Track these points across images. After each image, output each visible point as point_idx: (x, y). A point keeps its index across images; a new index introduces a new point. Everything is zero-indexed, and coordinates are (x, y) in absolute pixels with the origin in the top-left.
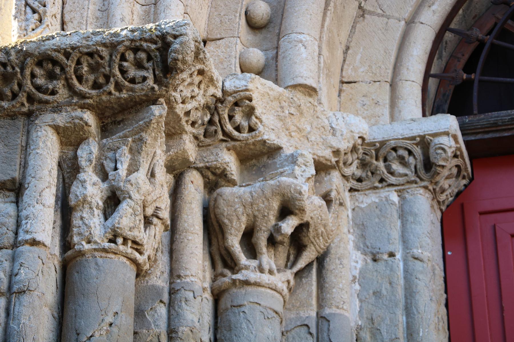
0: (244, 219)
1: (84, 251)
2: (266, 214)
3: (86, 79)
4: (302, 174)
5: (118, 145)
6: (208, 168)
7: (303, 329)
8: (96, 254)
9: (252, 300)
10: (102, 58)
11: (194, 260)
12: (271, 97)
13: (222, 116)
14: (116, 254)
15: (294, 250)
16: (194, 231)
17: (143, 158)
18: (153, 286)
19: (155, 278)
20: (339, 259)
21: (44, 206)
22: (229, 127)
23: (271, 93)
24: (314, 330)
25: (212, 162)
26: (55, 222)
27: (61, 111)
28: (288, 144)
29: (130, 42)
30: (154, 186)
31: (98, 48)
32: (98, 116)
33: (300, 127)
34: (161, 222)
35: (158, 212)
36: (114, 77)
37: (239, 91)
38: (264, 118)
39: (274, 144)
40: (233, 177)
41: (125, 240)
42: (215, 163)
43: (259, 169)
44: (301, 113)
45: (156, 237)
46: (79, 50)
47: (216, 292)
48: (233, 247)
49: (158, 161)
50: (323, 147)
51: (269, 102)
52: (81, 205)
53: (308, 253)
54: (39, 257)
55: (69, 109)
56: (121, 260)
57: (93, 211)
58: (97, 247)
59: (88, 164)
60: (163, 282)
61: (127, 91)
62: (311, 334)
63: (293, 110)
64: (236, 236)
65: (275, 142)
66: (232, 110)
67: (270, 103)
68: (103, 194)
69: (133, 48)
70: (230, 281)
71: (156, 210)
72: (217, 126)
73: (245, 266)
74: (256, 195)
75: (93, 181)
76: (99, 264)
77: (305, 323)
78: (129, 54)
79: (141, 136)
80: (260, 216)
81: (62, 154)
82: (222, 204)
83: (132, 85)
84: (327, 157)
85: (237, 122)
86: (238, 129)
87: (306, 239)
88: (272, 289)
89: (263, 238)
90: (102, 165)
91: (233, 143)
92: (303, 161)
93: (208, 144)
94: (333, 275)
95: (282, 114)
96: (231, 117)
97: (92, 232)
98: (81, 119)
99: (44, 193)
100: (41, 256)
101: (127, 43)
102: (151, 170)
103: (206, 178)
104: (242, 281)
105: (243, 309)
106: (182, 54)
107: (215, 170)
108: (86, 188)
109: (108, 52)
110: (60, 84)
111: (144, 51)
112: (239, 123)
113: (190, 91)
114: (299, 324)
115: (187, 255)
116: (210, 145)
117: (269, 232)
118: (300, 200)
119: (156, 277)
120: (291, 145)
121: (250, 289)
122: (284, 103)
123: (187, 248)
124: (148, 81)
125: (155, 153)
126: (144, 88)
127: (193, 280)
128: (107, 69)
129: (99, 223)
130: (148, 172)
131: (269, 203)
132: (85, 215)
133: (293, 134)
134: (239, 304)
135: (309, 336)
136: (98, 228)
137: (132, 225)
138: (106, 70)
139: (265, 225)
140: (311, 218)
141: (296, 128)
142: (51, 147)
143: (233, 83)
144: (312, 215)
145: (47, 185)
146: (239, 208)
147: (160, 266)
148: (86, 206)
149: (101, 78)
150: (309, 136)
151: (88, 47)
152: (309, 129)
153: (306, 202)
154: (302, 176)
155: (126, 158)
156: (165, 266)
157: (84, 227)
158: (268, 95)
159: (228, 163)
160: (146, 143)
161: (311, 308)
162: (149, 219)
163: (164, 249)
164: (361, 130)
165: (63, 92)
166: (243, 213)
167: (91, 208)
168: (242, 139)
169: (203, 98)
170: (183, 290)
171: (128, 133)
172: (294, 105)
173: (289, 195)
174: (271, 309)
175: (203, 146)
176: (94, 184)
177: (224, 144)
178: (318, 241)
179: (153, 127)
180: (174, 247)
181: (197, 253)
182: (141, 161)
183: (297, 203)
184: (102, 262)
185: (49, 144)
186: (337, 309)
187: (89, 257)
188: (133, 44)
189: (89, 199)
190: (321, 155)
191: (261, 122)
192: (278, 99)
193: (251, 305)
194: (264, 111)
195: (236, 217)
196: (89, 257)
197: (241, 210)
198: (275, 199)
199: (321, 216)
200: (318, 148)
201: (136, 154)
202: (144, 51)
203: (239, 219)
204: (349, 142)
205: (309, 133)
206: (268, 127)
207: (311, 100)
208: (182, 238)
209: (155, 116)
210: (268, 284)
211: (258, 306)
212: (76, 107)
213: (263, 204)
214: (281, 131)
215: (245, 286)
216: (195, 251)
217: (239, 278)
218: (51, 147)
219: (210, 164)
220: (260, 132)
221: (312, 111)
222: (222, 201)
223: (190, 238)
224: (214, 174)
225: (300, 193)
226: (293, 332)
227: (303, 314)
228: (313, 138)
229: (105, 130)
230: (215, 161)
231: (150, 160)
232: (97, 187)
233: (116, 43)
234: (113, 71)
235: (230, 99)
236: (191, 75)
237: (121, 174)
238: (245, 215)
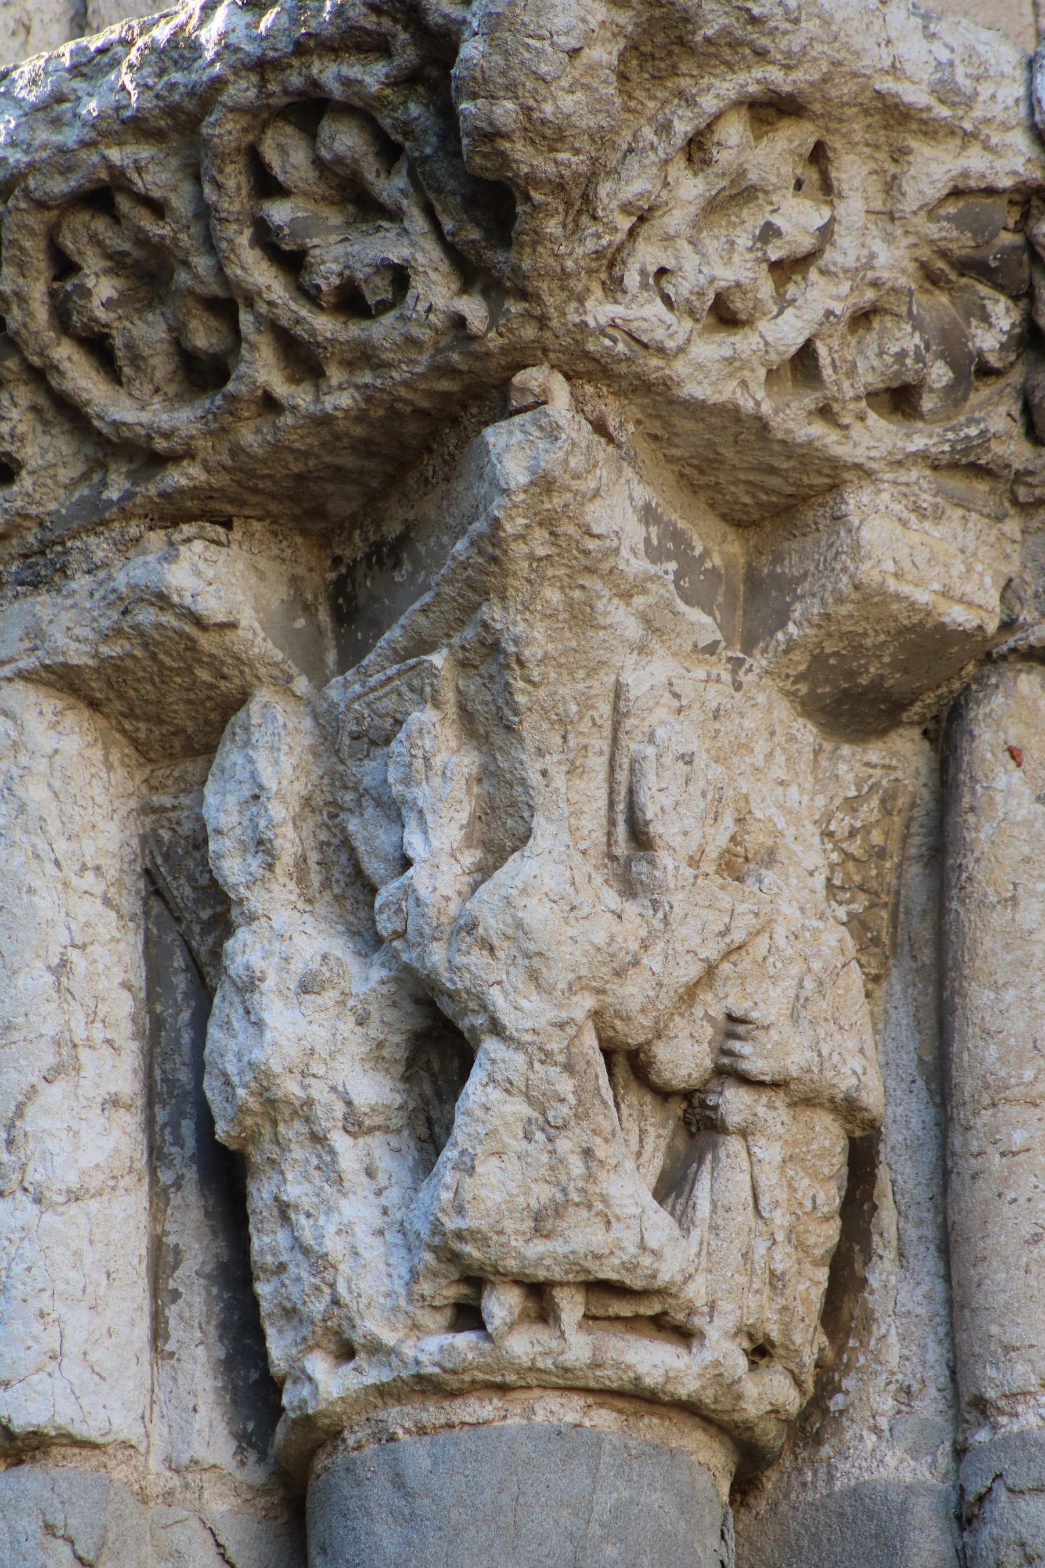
1: (324, 1414)
3: (127, 346)
5: (389, 704)
8: (397, 1417)
10: (158, 208)
14: (503, 1389)
17: (540, 753)
18: (856, 1493)
19: (870, 1440)
21: (38, 1201)
26: (161, 1261)
27: (63, 570)
29: (254, 78)
30: (655, 904)
31: (115, 155)
32: (305, 533)
34: (780, 1100)
35: (737, 1046)
36: (250, 304)
41: (539, 1297)
45: (764, 1201)
46: (26, 191)
49: (651, 739)
52: (267, 1131)
54: (49, 1529)
55: (100, 548)
56: (539, 1418)
57: (332, 1152)
58: (385, 1376)
59: (255, 863)
60: (914, 1452)
61: (350, 365)
68: (374, 1030)
69: (288, 106)
71: (732, 1035)
75: (297, 967)
76: (412, 1483)
78: (282, 149)
79: (485, 626)
81: (148, 820)
83: (355, 330)
90: (346, 844)
97: (342, 1289)
98: (162, 600)
99: (32, 1122)
100: (58, 1520)
101: (242, 90)
102: (621, 807)
106: (512, 89)
108: (259, 1025)
109: (174, 162)
110: (15, 414)
111: (347, 110)
113: (744, 241)
115: (1005, 1261)
119: (876, 1430)
123: (1008, 1211)
124: (418, 285)
125: (619, 691)
126: (416, 331)
128: (202, 263)
129: (379, 1222)
130: (612, 822)
132: (294, 1191)
136: (373, 1251)
137: (543, 1193)
138: (196, 277)
142: (51, 811)
145: (49, 1059)
147: (893, 1356)
148: (292, 1131)
149: (193, 324)
151: (63, 160)
155: (437, 781)
156: (923, 1347)
157: (300, 1269)
160: (521, 664)
162: (703, 1104)
163: (912, 1233)
165: (44, 452)
167: (318, 1139)
169: (889, 239)
170: (1003, 1496)
171: (421, 620)
176: (307, 986)
179: (531, 557)
180: (953, 1216)
182: (535, 778)
184: (427, 1463)
185: (36, 793)
187: (359, 1447)
188: (273, 87)
189: (291, 1087)
196: (359, 1447)
201: (499, 737)
202: (347, 110)
208: (974, 1147)
209: (506, 492)
212: (133, 530)
218: (51, 811)
223: (1019, 1138)
229: (347, 610)
231: (600, 743)
232: (330, 997)
233: (190, 105)
234: (233, 271)
236: (697, 149)
237: (423, 892)
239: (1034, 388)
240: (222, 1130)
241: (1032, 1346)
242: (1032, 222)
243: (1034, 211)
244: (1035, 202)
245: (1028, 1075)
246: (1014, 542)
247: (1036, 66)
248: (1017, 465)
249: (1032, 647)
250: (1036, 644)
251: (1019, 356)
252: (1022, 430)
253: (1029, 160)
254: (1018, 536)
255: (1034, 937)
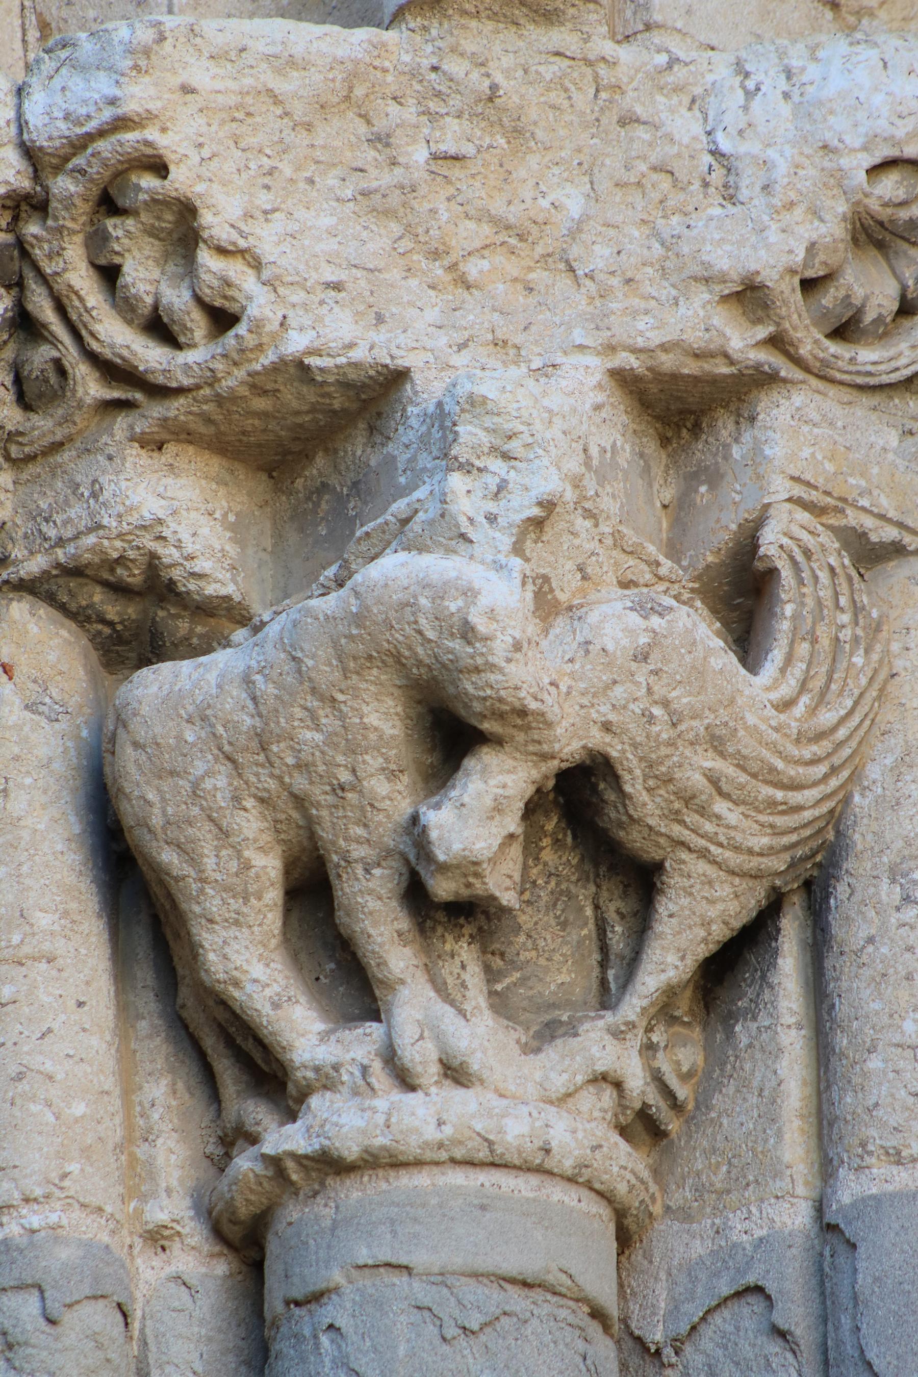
0: (250, 824)
2: (345, 776)
4: (491, 506)
6: (75, 571)
7: (746, 1310)
9: (364, 1255)
11: (34, 1108)
12: (299, 110)
13: (59, 286)
15: (625, 895)
16: (26, 949)
20: (894, 874)
22: (116, 335)
23: (281, 86)
24: (796, 1313)
25: (76, 537)
28: (442, 340)
33: (513, 214)
37: (90, 138)
38: (266, 239)
39: (355, 365)
40: (211, 589)
42: (91, 540)
43: (342, 501)
44: (517, 133)
47: (234, 1233)
48: (237, 984)
50: (667, 292)
51: (289, 137)
53: (685, 901)
62: (781, 1334)
63: (452, 135)
64: (237, 923)
65: (359, 354)
66: (97, 240)
67: (301, 139)
70: (259, 1168)
72: (53, 341)
73: (317, 1069)
74: (271, 690)
77: (751, 1279)
80: (319, 793)
82: (132, 769)
84: (696, 338)
85: (138, 299)
86: (160, 328)
87: (635, 835)
88: (470, 1163)
89: (372, 904)
91: (157, 410)
92: (485, 439)
93: (45, 442)
94: (866, 972)
95: (384, 179)
96: (109, 275)
103: (88, 619)
104: (306, 1157)
105: (328, 1313)
107: (112, 570)
112: (149, 300)
114: (726, 1291)
116: (57, 447)
117: (396, 863)
118: (477, 670)
120: (459, 337)
121: (352, 1193)
122: (393, 108)
127: (35, 1221)
131: (342, 717)
133: (474, 268)
134: (311, 1288)
135: (774, 1347)
139: (360, 831)
140: (607, 727)
141: (486, 229)
143: (59, 99)
144: (604, 711)
146: (208, 774)
150: (575, 251)
152: (574, 203)
153: (511, 668)
154: (492, 519)
158: (276, 100)
159: (160, 521)
161: (782, 1185)
164: (882, 125)
166: (236, 799)
168: (186, 382)
172: (456, 102)
173: (420, 650)
174: (476, 1275)
175: (31, 458)
177: (121, 423)
178: (709, 827)
181: (49, 1067)
183: (470, 689)
186: (895, 1169)
190: (656, 338)
191: (257, 265)
192: (349, 95)
193: (365, 1281)
194: (264, 200)
195: (208, 826)
197: (221, 781)
198: (368, 688)
199: (665, 704)
200: (636, 302)
203: (224, 833)
204: (815, 213)
205: (576, 231)
206: (301, 284)
207: (560, 37)
210: (441, 1145)
211: (400, 1280)
213: (318, 728)
214: (395, 274)
215: (329, 1181)
216: (36, 1061)
217: (287, 1147)
219: (71, 549)
220: (257, 327)
221: (583, 99)
222: (129, 750)
224: (119, 589)
225: (467, 633)
226: (708, 1338)
227: (743, 1229)
228: (599, 257)
230: (90, 530)
235: (63, 185)
238: (249, 803)
239: (23, 363)
240: (857, 1287)
241: (15, 1167)
242: (21, 224)
243: (23, 215)
244: (24, 207)
245: (16, 939)
246: (7, 491)
247: (24, 94)
248: (10, 427)
249: (21, 580)
250: (26, 577)
251: (11, 336)
252: (14, 398)
253: (18, 172)
254: (11, 487)
255: (22, 823)
